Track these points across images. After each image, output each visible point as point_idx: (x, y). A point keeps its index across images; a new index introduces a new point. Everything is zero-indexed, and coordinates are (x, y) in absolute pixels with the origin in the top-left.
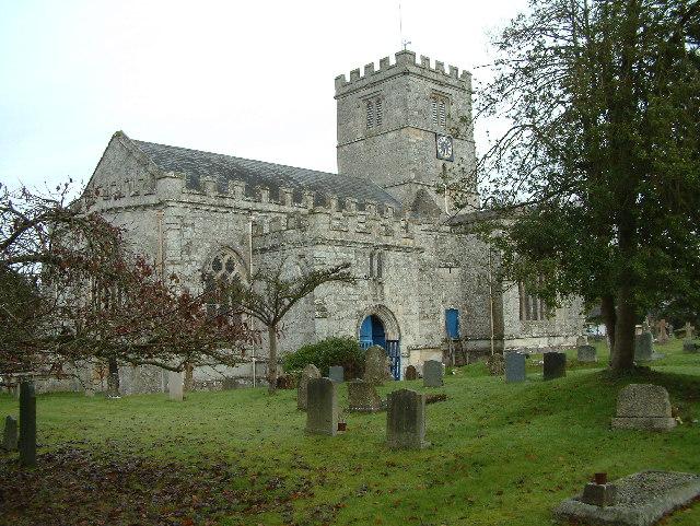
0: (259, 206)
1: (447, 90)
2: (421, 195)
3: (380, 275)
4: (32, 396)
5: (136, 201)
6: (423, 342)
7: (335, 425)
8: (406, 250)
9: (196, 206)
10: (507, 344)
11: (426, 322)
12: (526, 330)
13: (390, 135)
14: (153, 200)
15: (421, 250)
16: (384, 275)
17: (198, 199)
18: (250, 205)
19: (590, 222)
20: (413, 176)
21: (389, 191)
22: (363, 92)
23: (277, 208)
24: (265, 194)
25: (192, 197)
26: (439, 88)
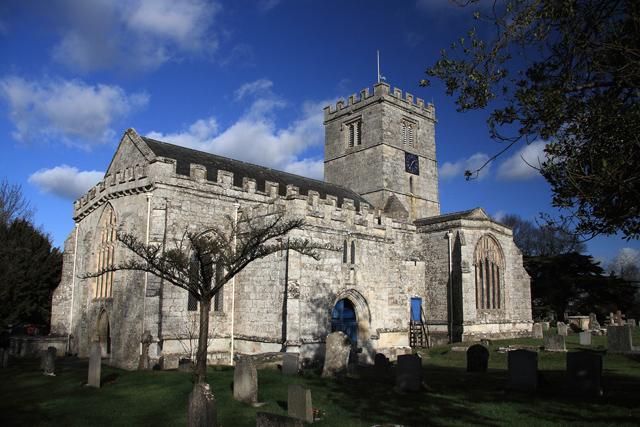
0: (246, 195)
1: (416, 118)
2: (392, 200)
3: (353, 262)
4: (178, 254)
5: (133, 185)
6: (392, 325)
7: (427, 167)
8: (377, 238)
9: (183, 189)
10: (466, 329)
11: (395, 307)
12: (481, 314)
13: (367, 151)
14: (144, 183)
15: (390, 241)
16: (357, 261)
17: (187, 183)
18: (237, 193)
19: (596, 312)
20: (385, 184)
21: (364, 197)
22: (402, 104)
23: (262, 198)
24: (252, 185)
25: (180, 181)
26: (408, 115)
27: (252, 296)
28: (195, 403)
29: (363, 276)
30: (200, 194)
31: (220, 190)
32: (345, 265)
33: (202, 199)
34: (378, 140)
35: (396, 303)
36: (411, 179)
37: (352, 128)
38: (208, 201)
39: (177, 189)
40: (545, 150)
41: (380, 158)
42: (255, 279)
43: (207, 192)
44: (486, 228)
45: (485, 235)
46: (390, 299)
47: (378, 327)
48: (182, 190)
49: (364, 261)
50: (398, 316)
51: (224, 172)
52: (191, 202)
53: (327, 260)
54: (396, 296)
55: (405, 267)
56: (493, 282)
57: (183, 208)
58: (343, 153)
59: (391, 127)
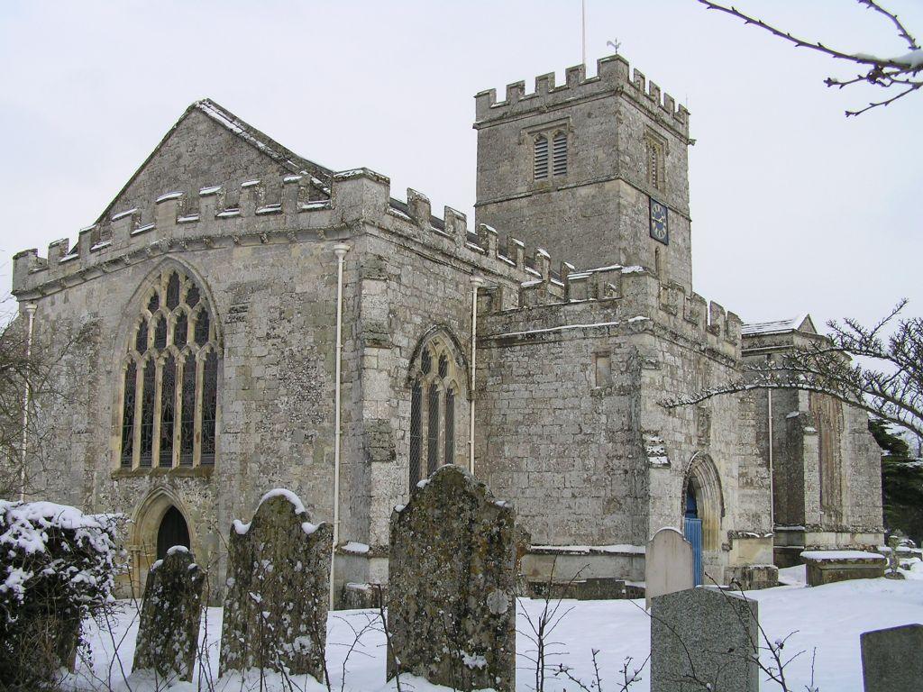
11: (748, 491)
13: (583, 191)
27: (529, 464)
28: (288, 632)
30: (427, 253)
33: (428, 263)
34: (608, 170)
35: (749, 484)
37: (541, 140)
38: (436, 268)
40: (692, 142)
41: (612, 206)
42: (533, 429)
46: (741, 475)
48: (401, 241)
50: (752, 507)
54: (752, 471)
56: (168, 417)
57: (404, 280)
58: (522, 189)
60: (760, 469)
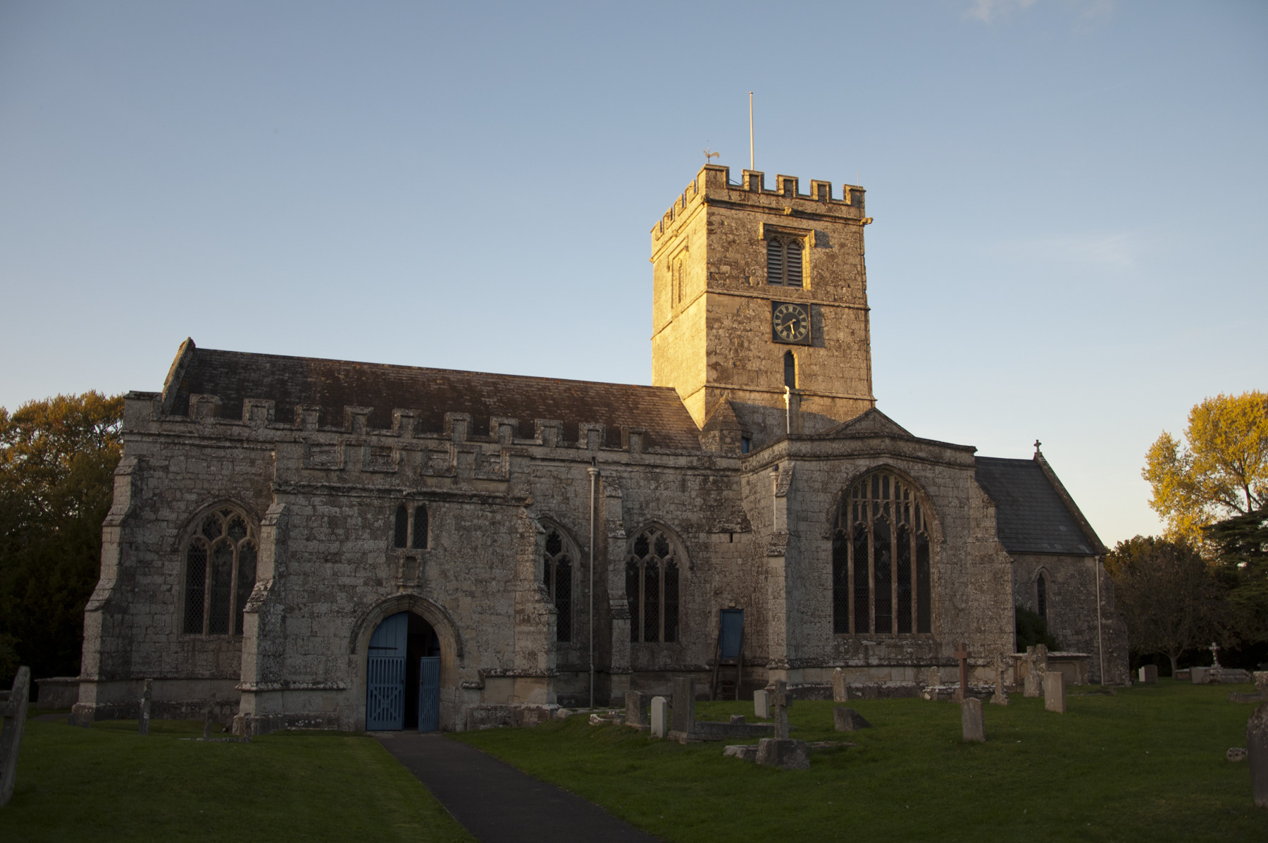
3: (420, 542)
25: (166, 426)
29: (444, 574)
30: (205, 443)
31: (246, 433)
32: (400, 551)
33: (209, 451)
36: (789, 357)
38: (222, 453)
39: (162, 440)
43: (218, 439)
44: (875, 454)
45: (868, 471)
47: (483, 666)
49: (445, 542)
51: (253, 401)
52: (187, 457)
53: (349, 545)
55: (706, 547)
57: (172, 469)
59: (731, 255)
60: (537, 606)
